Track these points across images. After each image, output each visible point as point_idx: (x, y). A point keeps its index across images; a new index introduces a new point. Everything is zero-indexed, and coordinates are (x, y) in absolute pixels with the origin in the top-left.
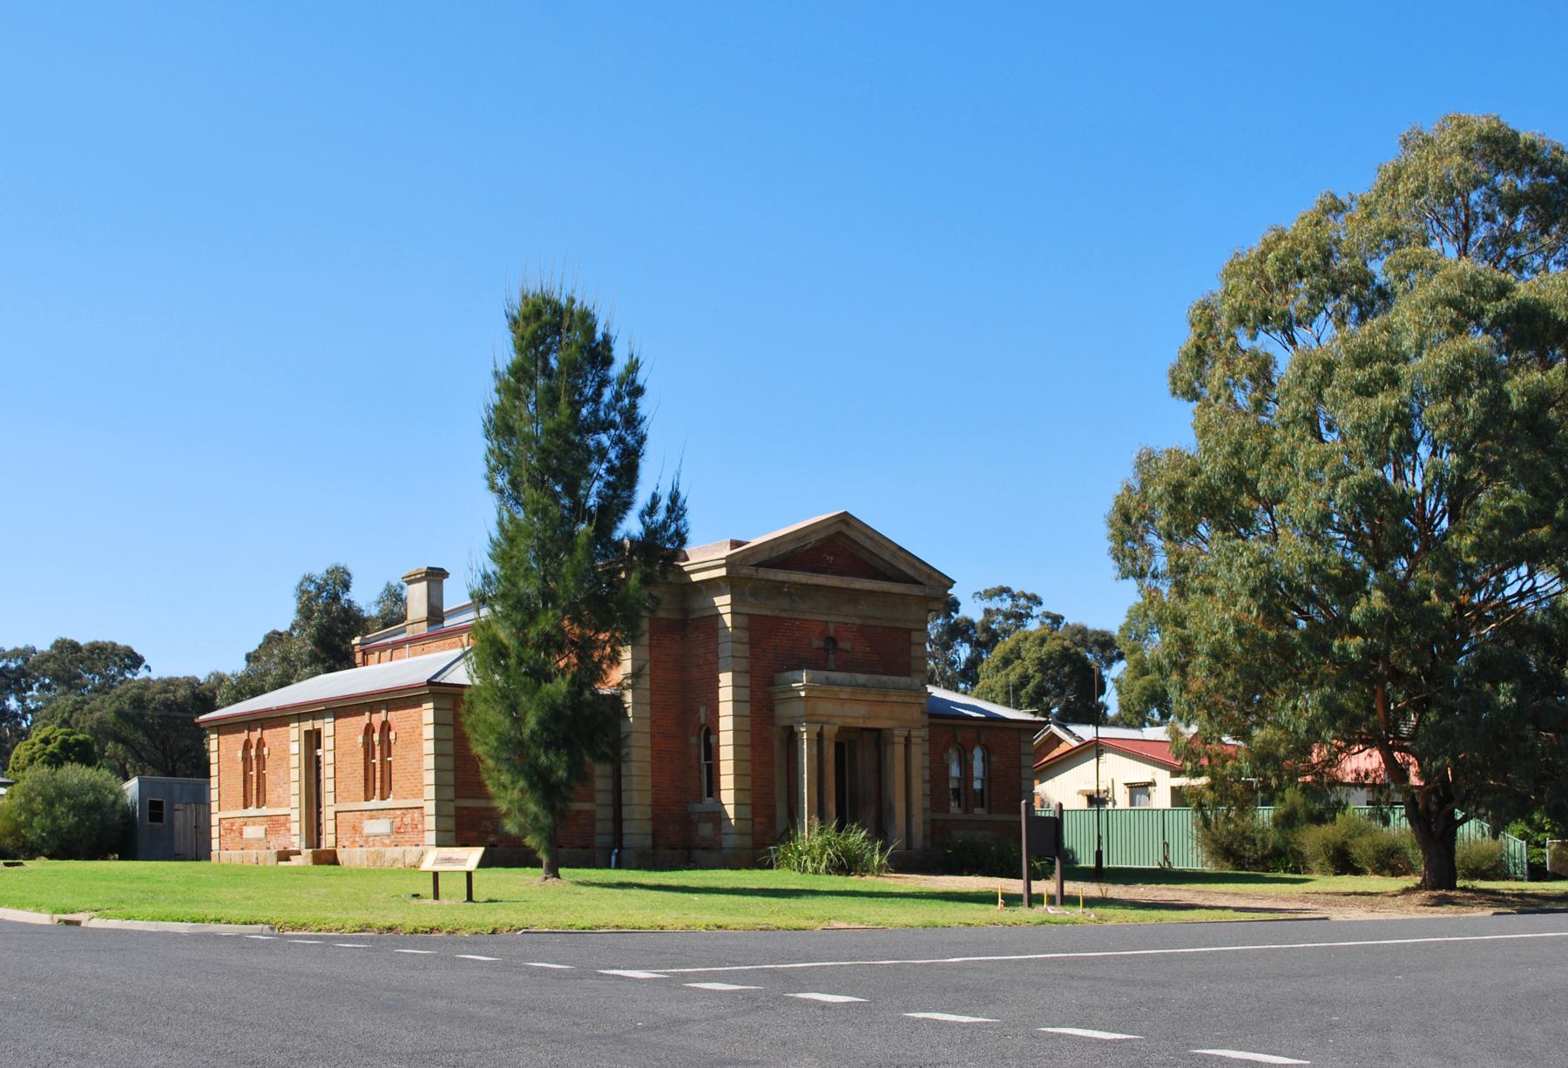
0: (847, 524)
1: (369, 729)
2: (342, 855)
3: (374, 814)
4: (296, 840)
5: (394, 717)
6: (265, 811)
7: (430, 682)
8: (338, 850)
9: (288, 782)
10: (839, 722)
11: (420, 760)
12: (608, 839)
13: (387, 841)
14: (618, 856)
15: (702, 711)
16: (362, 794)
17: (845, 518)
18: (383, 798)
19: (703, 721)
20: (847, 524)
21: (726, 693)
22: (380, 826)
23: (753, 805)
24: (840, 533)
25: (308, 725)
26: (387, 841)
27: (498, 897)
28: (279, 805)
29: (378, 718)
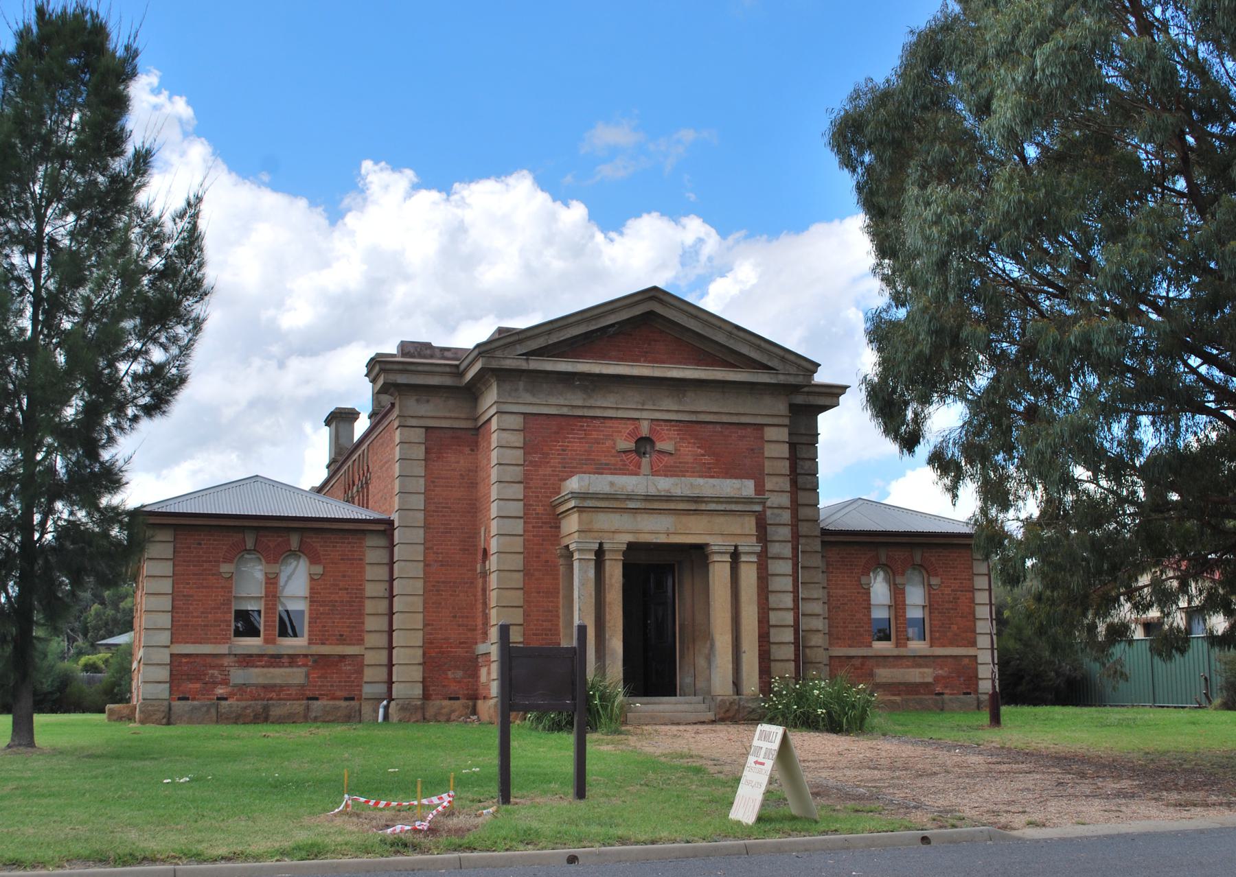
20: (661, 301)
24: (651, 314)
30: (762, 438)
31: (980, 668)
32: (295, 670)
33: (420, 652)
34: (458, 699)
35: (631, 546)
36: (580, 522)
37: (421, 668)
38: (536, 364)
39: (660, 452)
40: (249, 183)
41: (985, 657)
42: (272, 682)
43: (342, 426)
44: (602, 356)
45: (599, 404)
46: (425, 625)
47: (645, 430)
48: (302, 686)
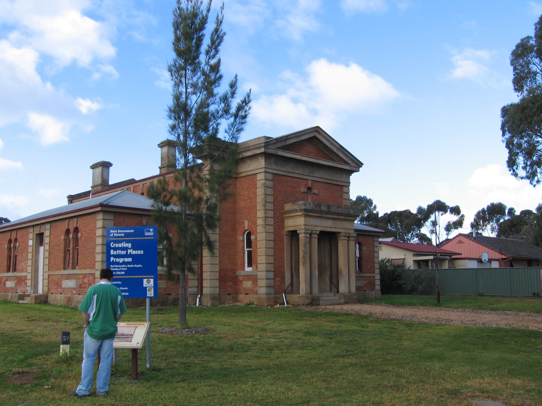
0: (318, 132)
1: (68, 232)
2: (51, 298)
3: (69, 277)
4: (29, 289)
5: (81, 223)
6: (16, 274)
7: (100, 203)
8: (50, 295)
9: (27, 260)
10: (319, 229)
11: (94, 248)
12: (195, 290)
13: (74, 292)
14: (200, 298)
15: (246, 223)
16: (62, 266)
17: (317, 129)
18: (74, 268)
19: (246, 228)
20: (318, 132)
21: (139, 266)
22: (69, 284)
23: (274, 271)
24: (315, 137)
25: (37, 230)
26: (74, 292)
27: (216, 15)
28: (22, 271)
29: (73, 224)
30: (342, 191)
31: (376, 281)
32: (162, 281)
33: (218, 274)
34: (230, 294)
35: (321, 232)
36: (305, 221)
37: (218, 281)
38: (281, 153)
39: (314, 194)
40: (334, 64)
41: (378, 277)
42: (421, 296)
43: (105, 169)
44: (297, 152)
45: (296, 172)
46: (220, 262)
47: (310, 184)
48: (165, 288)
